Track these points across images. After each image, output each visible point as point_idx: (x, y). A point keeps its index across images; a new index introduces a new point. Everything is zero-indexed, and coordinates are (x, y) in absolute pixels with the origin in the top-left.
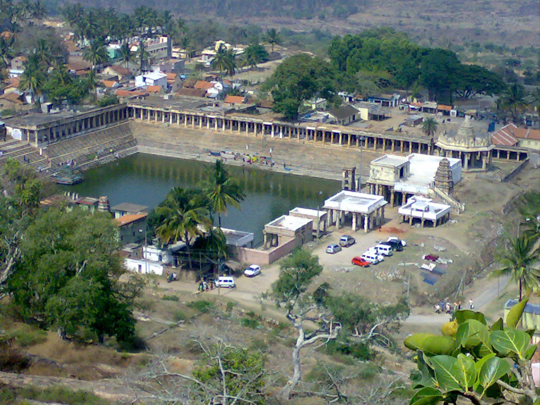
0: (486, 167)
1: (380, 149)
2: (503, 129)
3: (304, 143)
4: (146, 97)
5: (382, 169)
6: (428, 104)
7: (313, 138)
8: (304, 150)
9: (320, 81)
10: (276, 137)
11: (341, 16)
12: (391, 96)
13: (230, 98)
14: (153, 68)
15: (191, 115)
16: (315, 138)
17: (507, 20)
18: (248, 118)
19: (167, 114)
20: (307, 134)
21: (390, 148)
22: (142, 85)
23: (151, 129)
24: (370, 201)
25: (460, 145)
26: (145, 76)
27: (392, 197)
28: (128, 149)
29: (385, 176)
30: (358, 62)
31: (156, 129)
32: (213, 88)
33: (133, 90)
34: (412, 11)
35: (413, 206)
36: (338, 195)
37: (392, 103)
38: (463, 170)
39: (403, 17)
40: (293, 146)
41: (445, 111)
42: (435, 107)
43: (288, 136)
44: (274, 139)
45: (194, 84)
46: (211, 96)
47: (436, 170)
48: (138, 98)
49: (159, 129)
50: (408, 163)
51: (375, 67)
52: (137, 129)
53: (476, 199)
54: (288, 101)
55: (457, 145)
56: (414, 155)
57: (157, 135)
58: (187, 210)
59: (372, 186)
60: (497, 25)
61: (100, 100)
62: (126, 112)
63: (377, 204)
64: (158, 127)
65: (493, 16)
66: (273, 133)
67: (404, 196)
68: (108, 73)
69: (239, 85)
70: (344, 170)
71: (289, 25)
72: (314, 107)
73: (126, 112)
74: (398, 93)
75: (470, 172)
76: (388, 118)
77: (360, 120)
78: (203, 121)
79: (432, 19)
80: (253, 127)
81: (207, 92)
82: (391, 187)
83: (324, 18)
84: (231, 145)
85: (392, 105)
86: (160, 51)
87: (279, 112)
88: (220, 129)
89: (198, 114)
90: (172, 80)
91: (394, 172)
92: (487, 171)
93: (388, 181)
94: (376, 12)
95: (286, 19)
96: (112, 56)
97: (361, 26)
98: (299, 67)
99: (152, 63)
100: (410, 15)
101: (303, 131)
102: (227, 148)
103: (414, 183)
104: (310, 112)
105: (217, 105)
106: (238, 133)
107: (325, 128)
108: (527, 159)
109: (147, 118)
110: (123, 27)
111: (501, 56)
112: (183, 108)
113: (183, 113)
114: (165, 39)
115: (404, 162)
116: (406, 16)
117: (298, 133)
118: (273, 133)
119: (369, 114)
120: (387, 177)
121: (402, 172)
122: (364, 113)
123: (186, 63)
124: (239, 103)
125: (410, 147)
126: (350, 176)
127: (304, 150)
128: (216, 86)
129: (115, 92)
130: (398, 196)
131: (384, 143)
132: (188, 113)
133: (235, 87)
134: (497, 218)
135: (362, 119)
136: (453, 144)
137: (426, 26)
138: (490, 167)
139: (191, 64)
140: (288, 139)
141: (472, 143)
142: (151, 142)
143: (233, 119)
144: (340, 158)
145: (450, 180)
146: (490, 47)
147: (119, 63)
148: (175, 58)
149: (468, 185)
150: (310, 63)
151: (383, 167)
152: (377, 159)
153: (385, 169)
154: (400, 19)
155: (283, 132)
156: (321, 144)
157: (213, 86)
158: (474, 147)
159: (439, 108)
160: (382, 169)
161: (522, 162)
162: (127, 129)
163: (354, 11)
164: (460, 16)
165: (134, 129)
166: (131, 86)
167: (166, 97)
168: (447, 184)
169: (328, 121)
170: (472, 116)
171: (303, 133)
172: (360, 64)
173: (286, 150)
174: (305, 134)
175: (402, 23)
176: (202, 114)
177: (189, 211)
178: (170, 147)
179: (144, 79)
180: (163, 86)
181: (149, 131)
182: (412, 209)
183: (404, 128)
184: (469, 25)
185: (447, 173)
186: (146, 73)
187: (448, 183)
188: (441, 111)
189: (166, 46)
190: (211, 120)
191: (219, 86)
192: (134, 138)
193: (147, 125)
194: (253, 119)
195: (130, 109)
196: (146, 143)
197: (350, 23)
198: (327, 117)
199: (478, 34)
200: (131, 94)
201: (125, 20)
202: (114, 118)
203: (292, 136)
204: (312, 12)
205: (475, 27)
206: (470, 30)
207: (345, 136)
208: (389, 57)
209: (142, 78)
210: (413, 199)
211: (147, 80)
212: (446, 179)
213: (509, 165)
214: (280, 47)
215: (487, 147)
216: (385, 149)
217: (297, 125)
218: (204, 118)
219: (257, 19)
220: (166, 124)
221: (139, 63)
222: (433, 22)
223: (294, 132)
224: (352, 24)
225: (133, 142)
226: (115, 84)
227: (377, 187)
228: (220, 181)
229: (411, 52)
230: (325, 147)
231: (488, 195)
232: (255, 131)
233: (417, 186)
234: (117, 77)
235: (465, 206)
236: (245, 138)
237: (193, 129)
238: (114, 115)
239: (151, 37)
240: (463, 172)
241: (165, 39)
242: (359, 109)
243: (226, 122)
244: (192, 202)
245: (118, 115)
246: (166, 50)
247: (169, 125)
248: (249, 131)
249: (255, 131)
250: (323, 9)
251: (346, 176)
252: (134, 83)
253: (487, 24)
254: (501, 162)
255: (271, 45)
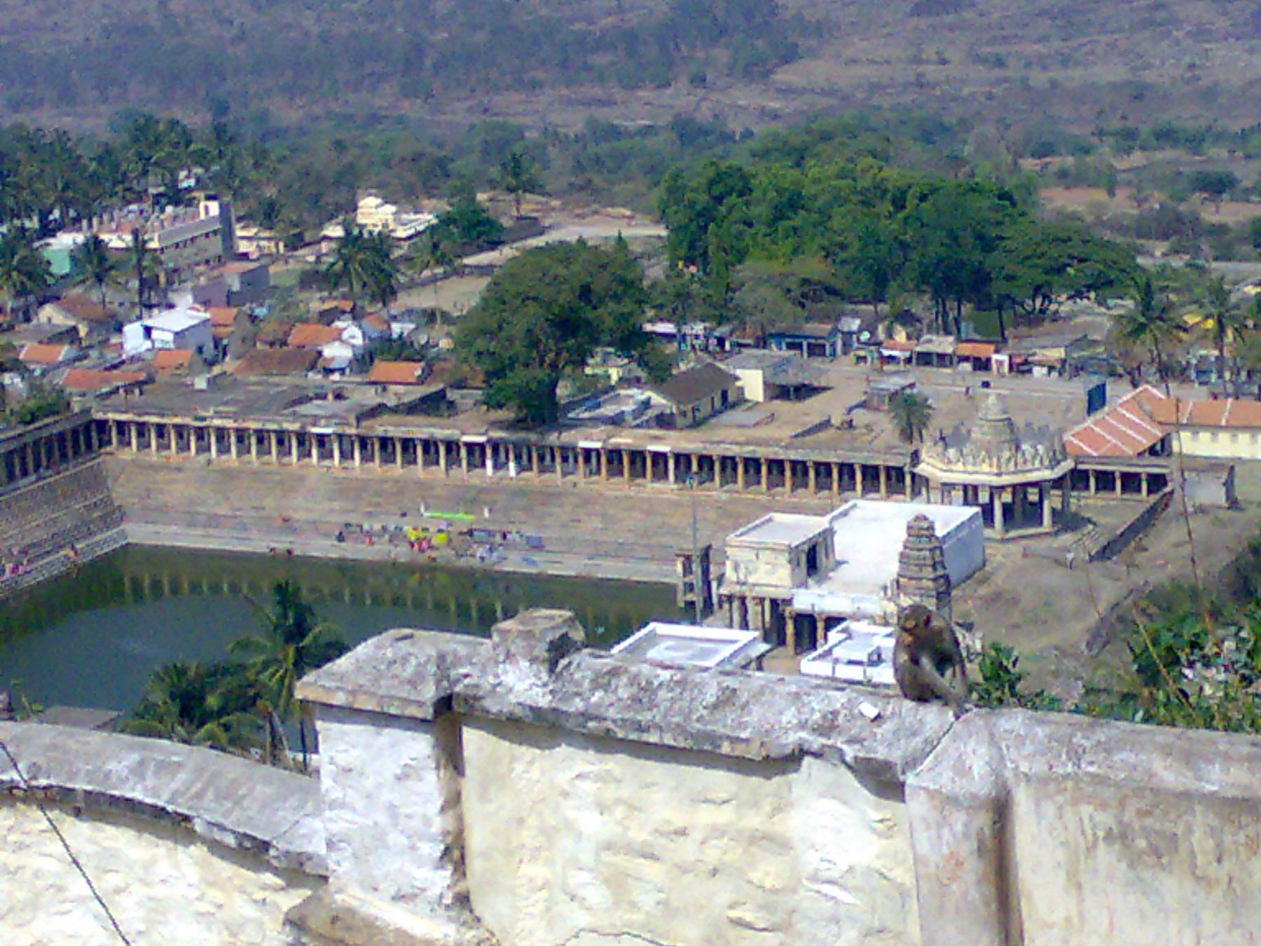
0: (1054, 523)
1: (779, 489)
2: (1121, 405)
3: (575, 485)
4: (146, 387)
5: (757, 556)
6: (930, 341)
7: (599, 471)
8: (577, 506)
9: (606, 315)
10: (501, 473)
11: (754, 71)
12: (829, 327)
13: (383, 369)
14: (173, 297)
15: (268, 431)
16: (604, 470)
17: (1219, 51)
18: (421, 428)
19: (201, 433)
20: (581, 460)
21: (806, 485)
22: (143, 349)
23: (161, 476)
24: (721, 646)
25: (978, 469)
26: (149, 323)
27: (790, 629)
28: (97, 538)
29: (767, 572)
30: (739, 236)
31: (174, 476)
32: (337, 344)
33: (115, 367)
34: (952, 43)
35: (837, 652)
36: (638, 635)
37: (833, 345)
38: (988, 532)
39: (928, 62)
40: (549, 497)
41: (977, 359)
42: (950, 350)
43: (531, 469)
44: (495, 480)
45: (287, 334)
46: (332, 366)
47: (900, 548)
48: (121, 391)
49: (179, 476)
50: (828, 534)
51: (787, 246)
52: (122, 479)
53: (1016, 618)
54: (519, 377)
55: (970, 468)
56: (854, 506)
57: (178, 491)
58: (202, 724)
59: (736, 604)
60: (1192, 66)
61: (17, 408)
62: (90, 435)
63: (742, 655)
64: (179, 469)
65: (1177, 43)
66: (489, 463)
67: (820, 625)
68: (50, 320)
69: (412, 326)
70: (678, 556)
71: (606, 110)
72: (615, 374)
73: (90, 435)
74: (855, 314)
75: (1013, 539)
76: (825, 389)
77: (741, 400)
78: (301, 443)
79: (1011, 62)
80: (437, 452)
81: (320, 353)
82: (784, 600)
83: (704, 80)
84: (379, 505)
85: (834, 354)
86: (202, 242)
87: (501, 406)
88: (348, 464)
89: (286, 426)
90: (226, 326)
91: (790, 562)
92: (1056, 534)
93: (776, 586)
94: (849, 53)
95: (598, 92)
96: (61, 266)
97: (807, 98)
98: (547, 280)
99: (170, 282)
100: (947, 55)
101: (567, 453)
102: (369, 514)
103: (847, 587)
104: (597, 392)
105: (338, 397)
106: (397, 469)
107: (629, 441)
108: (1167, 489)
109: (149, 446)
110: (94, 178)
111: (1198, 158)
112: (248, 409)
113: (244, 425)
114: (214, 207)
115: (817, 531)
116: (934, 57)
117: (558, 460)
118: (489, 463)
119: (766, 384)
120: (771, 576)
121: (813, 559)
122: (752, 382)
123: (272, 269)
124: (404, 381)
125: (859, 477)
126: (696, 568)
127: (577, 506)
128: (345, 335)
129: (60, 378)
130: (806, 624)
131: (788, 473)
132: (257, 425)
133: (401, 336)
134: (1070, 664)
135: (747, 401)
136: (960, 466)
137: (992, 84)
138: (1067, 521)
139: (283, 273)
140: (532, 476)
141: (1009, 460)
142: (162, 513)
143: (382, 434)
144: (673, 521)
145: (940, 572)
146: (1166, 136)
147: (79, 290)
148: (245, 256)
149: (999, 580)
150: (575, 268)
151: (758, 549)
152: (742, 530)
153: (765, 556)
154: (920, 69)
155: (518, 458)
156: (620, 487)
157: (339, 338)
158: (1014, 473)
159: (959, 353)
160: (757, 556)
161: (1154, 498)
162: (96, 481)
163: (789, 56)
164: (1088, 48)
165: (116, 479)
166: (111, 356)
167: (201, 383)
168: (931, 584)
169: (651, 413)
170: (1051, 368)
171: (571, 460)
172: (748, 240)
173: (528, 510)
174: (576, 461)
175: (923, 80)
176: (296, 426)
177: (208, 726)
178: (214, 521)
179: (148, 331)
180: (200, 350)
181: (155, 482)
182: (836, 661)
183: (861, 417)
184: (1110, 73)
185: (927, 553)
186: (156, 311)
187: (935, 580)
188: (966, 359)
189: (218, 226)
190: (322, 440)
191: (353, 334)
192: (117, 504)
193: (153, 467)
194: (432, 430)
195: (102, 425)
196: (148, 516)
197: (779, 91)
198: (646, 404)
199: (1137, 97)
200: (106, 381)
201: (100, 160)
202: (57, 454)
203: (542, 471)
204: (670, 65)
205: (1129, 76)
206: (1114, 87)
207: (682, 460)
208: (825, 215)
209: (141, 331)
210: (843, 631)
211: (155, 334)
212: (928, 572)
213: (1111, 511)
214: (543, 199)
215: (1052, 468)
216: (793, 489)
217: (553, 438)
218: (302, 438)
219: (514, 97)
220: (202, 458)
221: (135, 284)
222: (1013, 71)
223: (548, 458)
224: (786, 91)
225: (113, 515)
226: (64, 351)
227: (750, 604)
228: (299, 630)
229: (889, 196)
230: (632, 494)
231: (1047, 604)
232: (442, 461)
233: (853, 595)
234: (74, 329)
235: (981, 639)
236: (420, 484)
237: (275, 467)
238: (56, 445)
239: (177, 203)
240: (989, 539)
241: (214, 207)
242: (739, 372)
243: (364, 442)
244: (212, 701)
245: (69, 444)
246: (219, 237)
247: (209, 462)
248: (427, 463)
249: (442, 461)
250: (700, 54)
251: (687, 570)
252: (121, 345)
253: (1163, 66)
254: (1100, 503)
255: (512, 197)
